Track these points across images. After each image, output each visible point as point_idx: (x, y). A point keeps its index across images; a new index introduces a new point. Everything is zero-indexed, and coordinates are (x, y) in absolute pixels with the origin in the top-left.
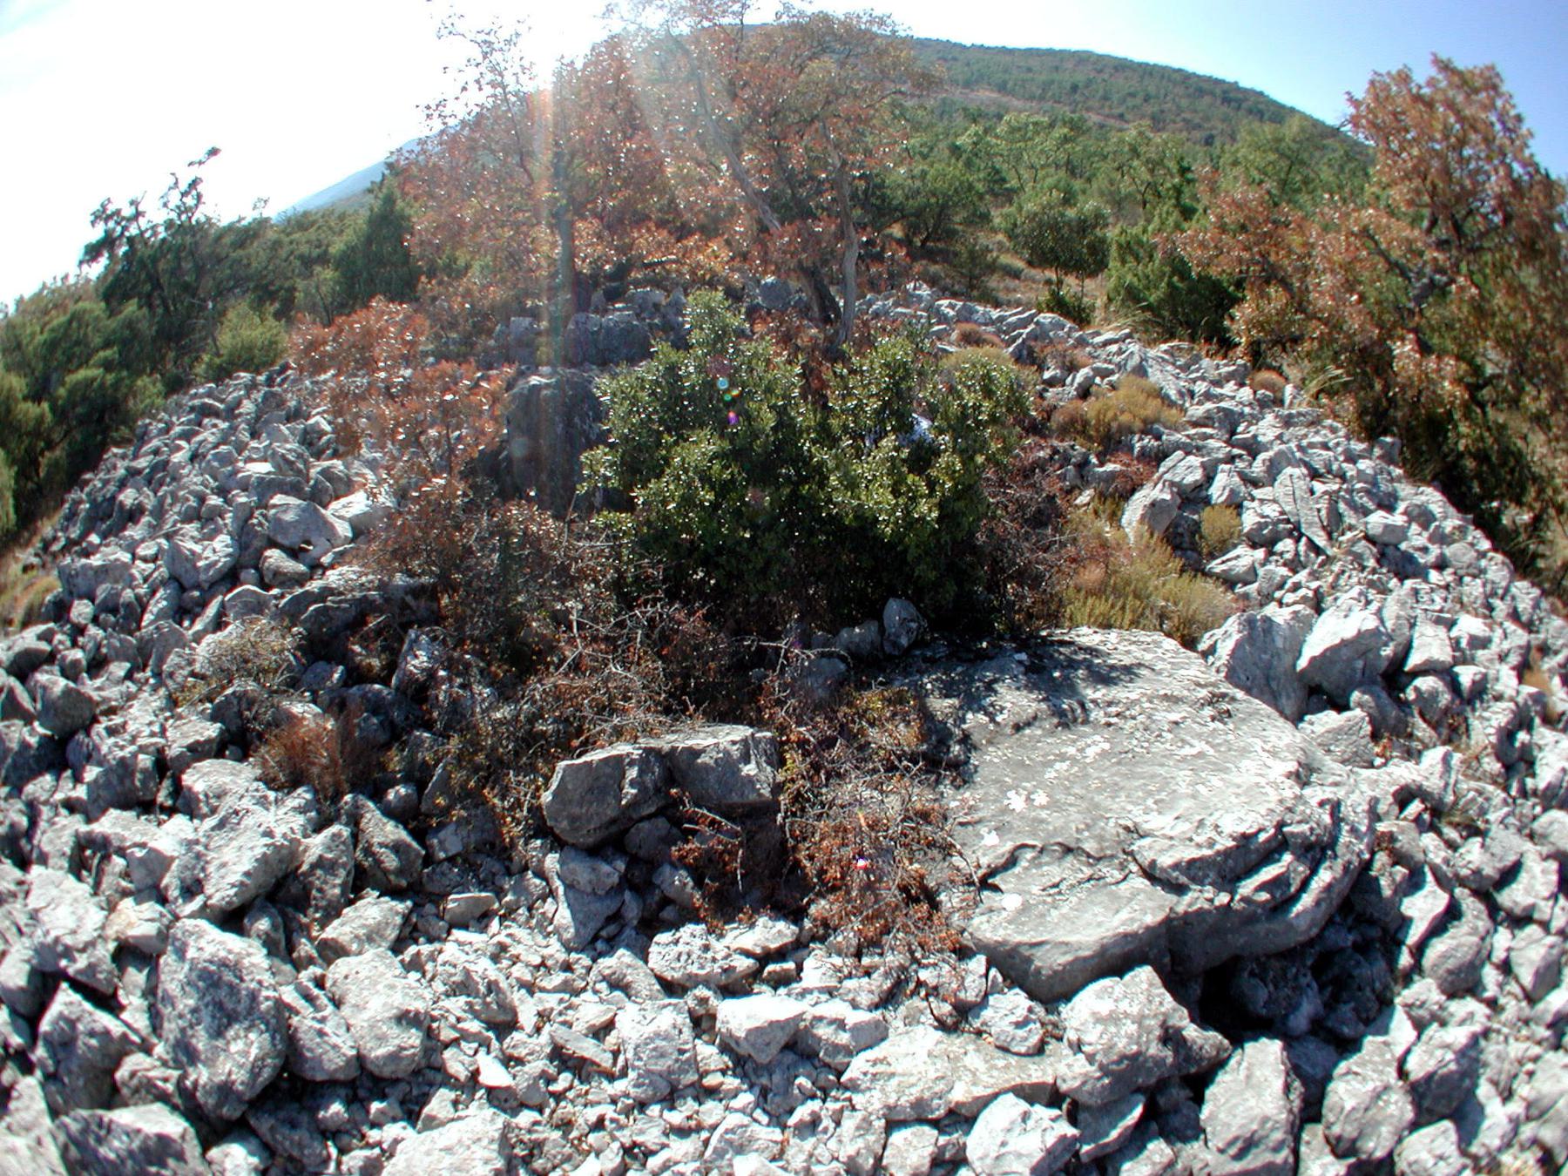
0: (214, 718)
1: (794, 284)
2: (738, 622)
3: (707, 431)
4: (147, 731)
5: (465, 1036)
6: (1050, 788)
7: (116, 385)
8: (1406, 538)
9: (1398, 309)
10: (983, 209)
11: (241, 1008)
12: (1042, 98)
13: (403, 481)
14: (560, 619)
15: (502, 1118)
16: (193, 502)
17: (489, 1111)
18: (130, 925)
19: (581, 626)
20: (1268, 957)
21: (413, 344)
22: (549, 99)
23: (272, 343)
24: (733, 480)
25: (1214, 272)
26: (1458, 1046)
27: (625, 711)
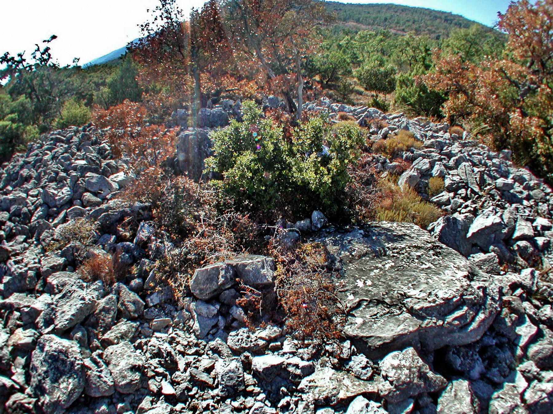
0: (62, 256)
1: (280, 98)
2: (260, 219)
3: (249, 151)
4: (33, 262)
5: (158, 374)
6: (372, 279)
7: (18, 128)
8: (513, 188)
9: (513, 100)
10: (349, 69)
11: (66, 369)
12: (373, 24)
13: (138, 168)
14: (197, 218)
15: (170, 407)
16: (53, 175)
17: (165, 405)
18: (20, 339)
19: (204, 220)
20: (460, 346)
21: (141, 118)
22: (188, 24)
23: (84, 115)
24: (258, 169)
25: (436, 90)
26: (548, 392)
27: (220, 251)
